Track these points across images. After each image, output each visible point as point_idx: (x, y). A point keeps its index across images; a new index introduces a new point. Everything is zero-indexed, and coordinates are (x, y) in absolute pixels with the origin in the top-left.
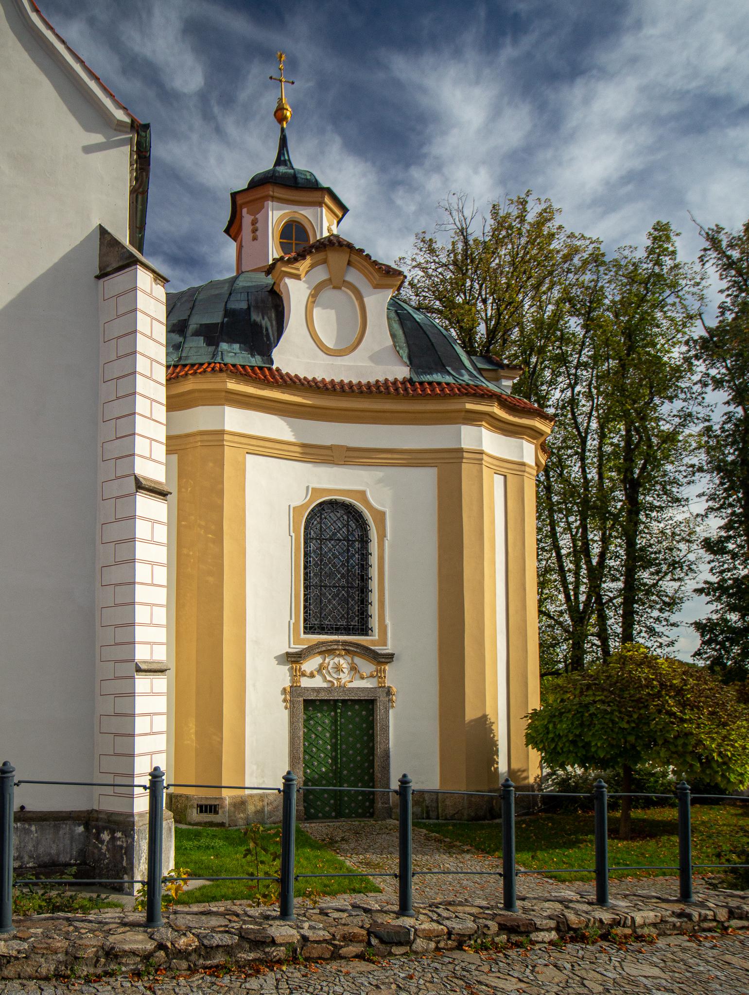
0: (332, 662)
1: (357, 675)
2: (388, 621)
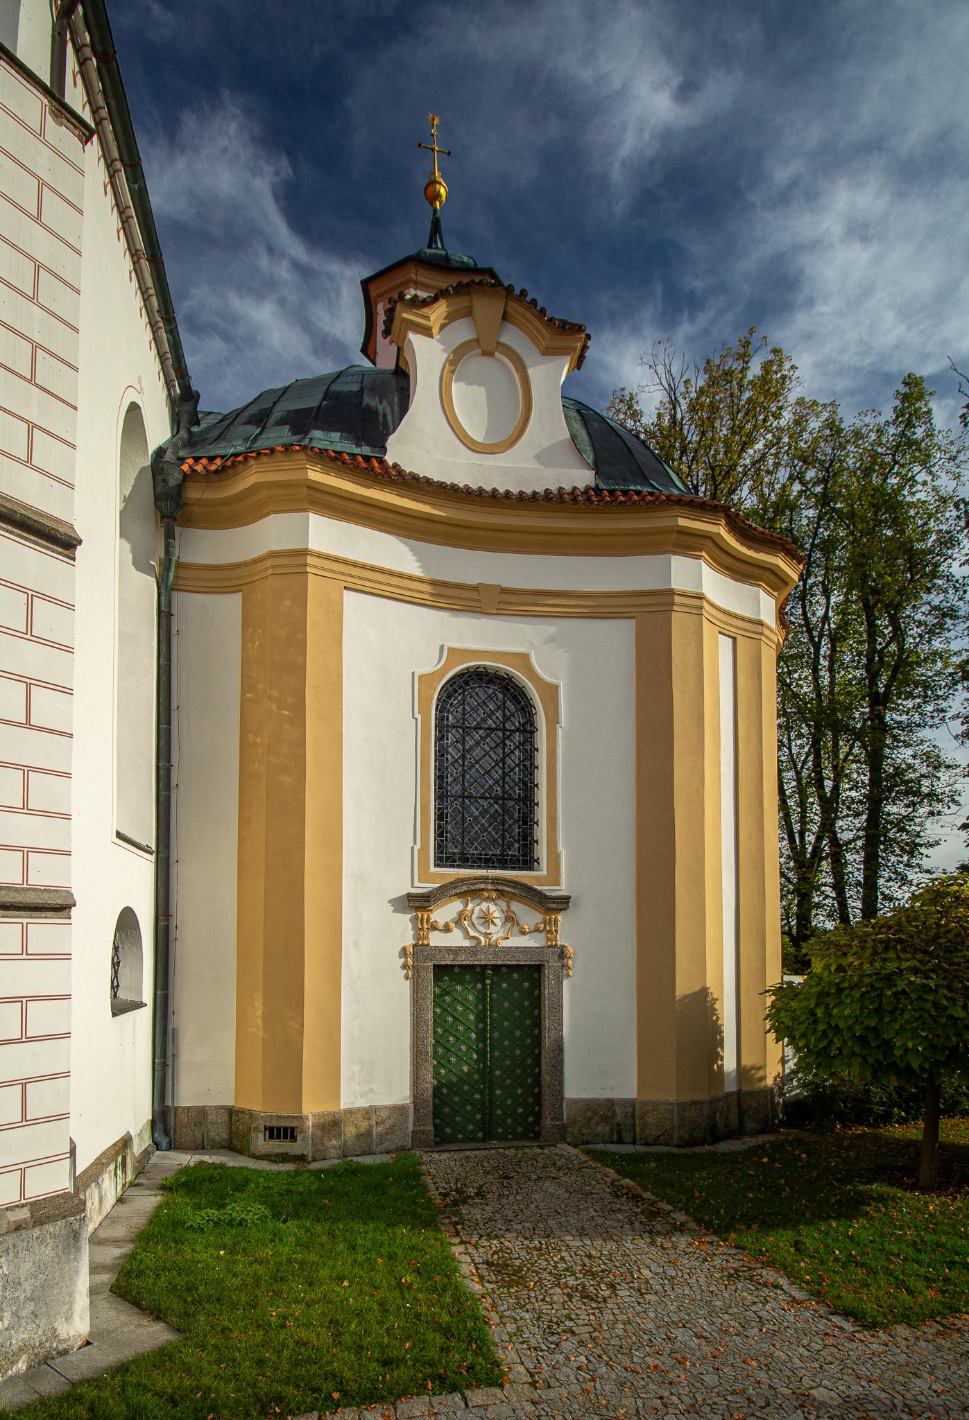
0: (477, 909)
1: (516, 929)
2: (561, 849)
